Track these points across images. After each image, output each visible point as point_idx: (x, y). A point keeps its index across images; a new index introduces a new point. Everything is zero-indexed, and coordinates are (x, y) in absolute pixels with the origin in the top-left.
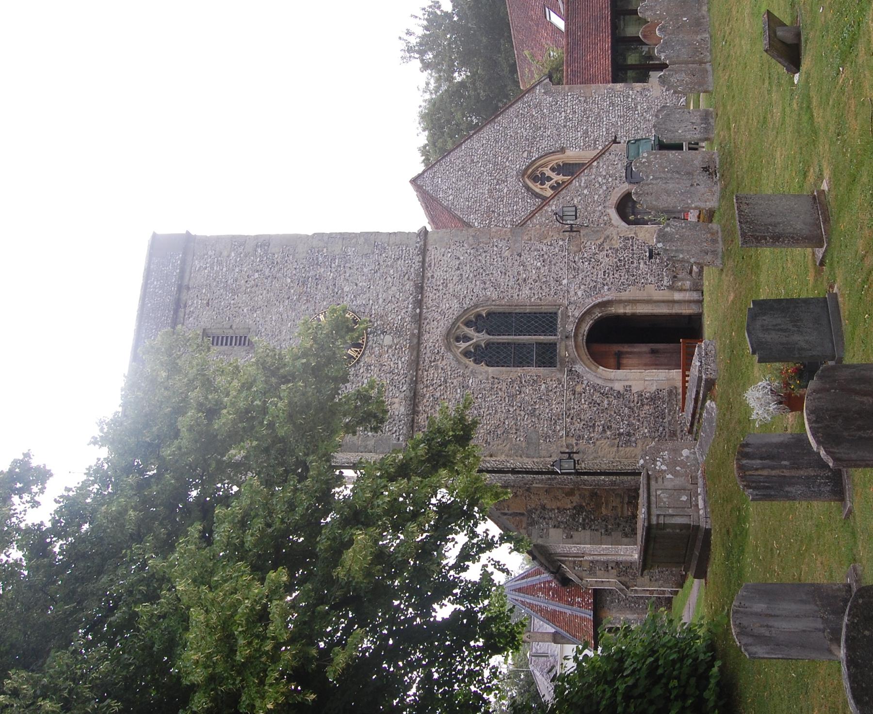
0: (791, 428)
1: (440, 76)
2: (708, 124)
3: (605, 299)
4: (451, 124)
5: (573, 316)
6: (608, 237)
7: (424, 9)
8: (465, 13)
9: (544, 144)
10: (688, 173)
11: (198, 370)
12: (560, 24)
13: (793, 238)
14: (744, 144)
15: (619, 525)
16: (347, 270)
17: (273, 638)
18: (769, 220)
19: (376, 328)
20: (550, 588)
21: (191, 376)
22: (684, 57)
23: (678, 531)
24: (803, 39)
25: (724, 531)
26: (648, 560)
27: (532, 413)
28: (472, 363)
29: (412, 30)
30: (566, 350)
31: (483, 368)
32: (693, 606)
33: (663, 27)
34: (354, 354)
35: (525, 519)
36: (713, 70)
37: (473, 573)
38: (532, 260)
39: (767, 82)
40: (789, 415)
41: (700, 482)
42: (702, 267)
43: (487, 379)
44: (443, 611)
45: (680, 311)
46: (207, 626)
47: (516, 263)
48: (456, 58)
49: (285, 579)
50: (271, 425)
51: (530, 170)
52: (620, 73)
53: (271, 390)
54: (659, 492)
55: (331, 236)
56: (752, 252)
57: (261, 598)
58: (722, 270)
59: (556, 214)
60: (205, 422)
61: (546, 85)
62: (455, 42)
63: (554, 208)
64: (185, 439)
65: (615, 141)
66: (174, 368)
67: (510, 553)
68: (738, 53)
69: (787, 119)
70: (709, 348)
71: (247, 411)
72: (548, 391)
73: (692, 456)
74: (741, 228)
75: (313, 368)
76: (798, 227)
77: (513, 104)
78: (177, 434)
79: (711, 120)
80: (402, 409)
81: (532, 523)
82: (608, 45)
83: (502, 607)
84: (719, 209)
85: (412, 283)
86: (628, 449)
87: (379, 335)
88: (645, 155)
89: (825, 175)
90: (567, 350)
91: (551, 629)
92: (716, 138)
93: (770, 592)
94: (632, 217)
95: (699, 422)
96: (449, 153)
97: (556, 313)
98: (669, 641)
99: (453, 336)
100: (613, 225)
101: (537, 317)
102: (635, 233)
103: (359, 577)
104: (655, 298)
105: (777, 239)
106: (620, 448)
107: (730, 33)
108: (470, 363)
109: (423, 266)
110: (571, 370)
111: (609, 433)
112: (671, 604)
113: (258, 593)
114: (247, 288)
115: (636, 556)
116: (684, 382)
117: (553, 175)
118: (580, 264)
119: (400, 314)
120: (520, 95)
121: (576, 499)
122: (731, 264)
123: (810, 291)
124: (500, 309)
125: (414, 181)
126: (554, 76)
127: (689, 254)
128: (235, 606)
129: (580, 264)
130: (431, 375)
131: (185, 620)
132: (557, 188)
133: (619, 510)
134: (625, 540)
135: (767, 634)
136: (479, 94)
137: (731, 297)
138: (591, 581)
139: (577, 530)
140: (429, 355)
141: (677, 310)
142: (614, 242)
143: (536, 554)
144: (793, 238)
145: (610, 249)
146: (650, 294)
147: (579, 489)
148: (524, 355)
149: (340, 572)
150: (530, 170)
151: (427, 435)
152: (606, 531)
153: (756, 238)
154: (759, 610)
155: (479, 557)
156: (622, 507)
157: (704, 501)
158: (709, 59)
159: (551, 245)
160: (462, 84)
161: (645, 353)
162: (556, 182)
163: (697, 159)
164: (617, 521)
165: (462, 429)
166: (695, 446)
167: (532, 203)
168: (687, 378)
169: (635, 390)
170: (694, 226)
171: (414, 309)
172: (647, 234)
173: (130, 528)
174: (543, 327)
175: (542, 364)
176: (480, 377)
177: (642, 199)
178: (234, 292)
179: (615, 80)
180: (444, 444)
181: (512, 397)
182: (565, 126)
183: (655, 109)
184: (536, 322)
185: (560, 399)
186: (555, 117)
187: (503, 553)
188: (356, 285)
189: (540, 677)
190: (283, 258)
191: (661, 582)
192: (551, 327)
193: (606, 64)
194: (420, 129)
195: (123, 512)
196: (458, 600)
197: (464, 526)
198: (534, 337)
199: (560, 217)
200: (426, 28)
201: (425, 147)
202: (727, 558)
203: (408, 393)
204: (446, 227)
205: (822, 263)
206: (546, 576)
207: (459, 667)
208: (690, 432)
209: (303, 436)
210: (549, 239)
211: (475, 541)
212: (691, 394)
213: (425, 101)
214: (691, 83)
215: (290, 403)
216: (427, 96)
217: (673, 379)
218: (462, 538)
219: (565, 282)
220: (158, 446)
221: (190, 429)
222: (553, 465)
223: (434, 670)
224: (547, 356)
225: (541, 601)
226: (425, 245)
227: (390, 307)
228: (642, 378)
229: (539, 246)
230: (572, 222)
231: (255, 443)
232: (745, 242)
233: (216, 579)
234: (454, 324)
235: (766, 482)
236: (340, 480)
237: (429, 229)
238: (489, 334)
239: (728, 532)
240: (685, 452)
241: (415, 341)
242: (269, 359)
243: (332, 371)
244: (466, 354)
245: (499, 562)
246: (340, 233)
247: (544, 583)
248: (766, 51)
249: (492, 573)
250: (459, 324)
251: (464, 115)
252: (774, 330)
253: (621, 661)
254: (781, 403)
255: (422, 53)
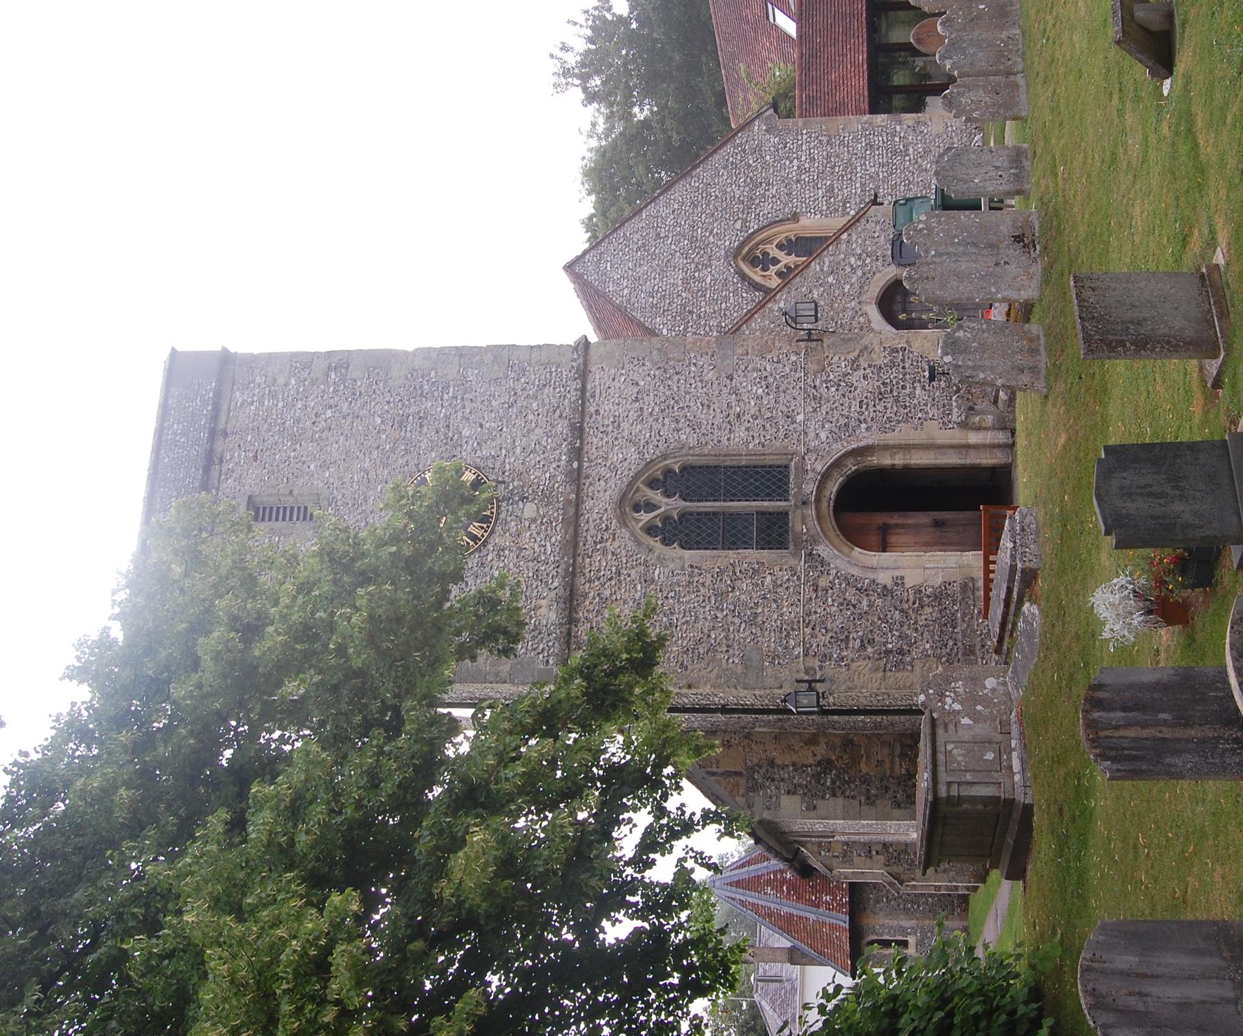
0: (1167, 651)
1: (612, 112)
2: (1021, 168)
3: (862, 444)
4: (627, 181)
5: (813, 470)
6: (866, 348)
7: (586, 12)
8: (648, 18)
9: (767, 208)
10: (991, 246)
11: (234, 562)
12: (788, 26)
13: (1168, 342)
14: (1079, 198)
15: (887, 788)
16: (467, 403)
17: (338, 1002)
18: (1129, 314)
19: (511, 492)
20: (784, 881)
21: (223, 571)
22: (983, 65)
23: (980, 807)
24: (1177, 22)
25: (1054, 809)
26: (935, 849)
27: (752, 621)
28: (659, 545)
29: (570, 43)
30: (804, 523)
31: (675, 551)
32: (1002, 921)
33: (948, 20)
34: (478, 533)
35: (742, 781)
36: (1028, 85)
37: (663, 871)
38: (749, 385)
39: (1116, 96)
40: (1163, 632)
41: (1015, 729)
42: (1014, 393)
43: (683, 568)
44: (618, 930)
45: (978, 461)
46: (232, 982)
47: (725, 390)
48: (635, 86)
49: (354, 907)
50: (341, 650)
51: (746, 249)
52: (881, 98)
53: (341, 596)
54: (949, 747)
55: (441, 351)
56: (1095, 367)
57: (317, 938)
58: (1046, 397)
59: (785, 314)
60: (241, 646)
61: (768, 118)
62: (634, 61)
63: (782, 305)
64: (209, 673)
65: (875, 202)
66: (195, 560)
67: (719, 839)
68: (1068, 57)
69: (1152, 154)
70: (1027, 521)
71: (306, 627)
72: (776, 585)
73: (1001, 688)
74: (1084, 328)
75: (407, 561)
76: (1177, 325)
77: (720, 147)
78: (196, 664)
79: (1025, 163)
80: (553, 616)
81: (754, 788)
82: (862, 57)
83: (708, 922)
84: (1041, 300)
85: (566, 422)
86: (899, 675)
87: (517, 503)
88: (923, 218)
89: (1220, 239)
90: (804, 522)
91: (784, 943)
92: (1034, 189)
93: (1144, 936)
94: (902, 317)
95: (1011, 635)
96: (622, 224)
97: (787, 467)
98: (969, 985)
99: (629, 504)
100: (873, 330)
101: (758, 473)
102: (907, 342)
103: (475, 899)
104: (939, 442)
105: (1144, 344)
106: (889, 674)
107: (1054, 25)
108: (655, 543)
109: (583, 396)
110: (810, 554)
111: (870, 650)
112: (968, 904)
113: (313, 930)
114: (314, 433)
115: (915, 835)
116: (987, 572)
117: (780, 255)
118: (823, 391)
119: (549, 469)
120: (730, 136)
121: (821, 750)
122: (1060, 387)
123: (1195, 430)
124: (702, 461)
125: (569, 268)
126: (782, 105)
127: (994, 371)
128: (276, 949)
129: (823, 391)
130: (596, 563)
131: (199, 962)
132: (787, 275)
133: (888, 765)
134: (897, 812)
135: (1141, 1007)
136: (670, 137)
137: (1062, 440)
138: (846, 873)
139: (823, 798)
140: (592, 532)
141: (973, 459)
142: (874, 356)
143: (761, 834)
144: (1168, 342)
145: (870, 366)
146: (931, 436)
147: (825, 734)
148: (739, 531)
149: (444, 889)
150: (746, 249)
151: (586, 660)
152: (868, 798)
153: (1109, 345)
154: (1125, 967)
155: (672, 847)
156: (892, 762)
157: (1022, 760)
158: (1020, 67)
159: (778, 362)
160: (645, 124)
161: (924, 526)
162: (786, 266)
163: (1004, 223)
164: (885, 783)
165: (642, 650)
166: (1006, 672)
167: (750, 298)
168: (992, 567)
169: (909, 583)
170: (1000, 329)
171: (570, 461)
172: (926, 344)
173: (120, 816)
174: (768, 487)
175: (765, 544)
176: (672, 566)
177: (919, 288)
178: (295, 439)
179: (874, 110)
180: (614, 673)
181: (721, 595)
182: (798, 181)
183: (936, 152)
184: (757, 480)
185: (795, 598)
186: (784, 167)
187: (708, 841)
188: (481, 426)
189: (771, 1012)
190: (370, 386)
191: (952, 873)
192: (780, 487)
193: (860, 84)
194: (584, 193)
195: (108, 790)
196: (639, 914)
197: (647, 799)
198: (753, 503)
199: (792, 318)
200: (591, 40)
201: (590, 218)
202: (1060, 852)
203: (561, 591)
204: (619, 336)
205: (1217, 384)
206: (775, 863)
207: (642, 1018)
208: (998, 651)
209: (391, 668)
210: (775, 353)
211: (664, 821)
212: (999, 593)
213: (591, 150)
214: (994, 105)
215: (371, 616)
216: (594, 143)
217: (969, 566)
218: (643, 818)
219: (800, 418)
220: (168, 682)
221: (217, 657)
222: (785, 701)
223: (603, 1022)
224: (773, 533)
225: (769, 899)
226: (586, 363)
227: (533, 459)
228: (920, 565)
229: (759, 363)
230: (810, 326)
231: (317, 678)
232: (1090, 351)
233: (249, 901)
234: (630, 485)
235: (1131, 749)
236: (454, 727)
237: (593, 338)
238: (685, 500)
239: (1061, 810)
240: (990, 683)
241: (572, 511)
242: (339, 546)
243: (438, 561)
244: (650, 530)
245: (702, 853)
246: (456, 348)
247: (775, 873)
248: (1118, 43)
249: (692, 870)
250: (639, 484)
251: (648, 170)
252: (1142, 494)
253: (894, 1014)
254: (1150, 612)
255: (585, 78)
